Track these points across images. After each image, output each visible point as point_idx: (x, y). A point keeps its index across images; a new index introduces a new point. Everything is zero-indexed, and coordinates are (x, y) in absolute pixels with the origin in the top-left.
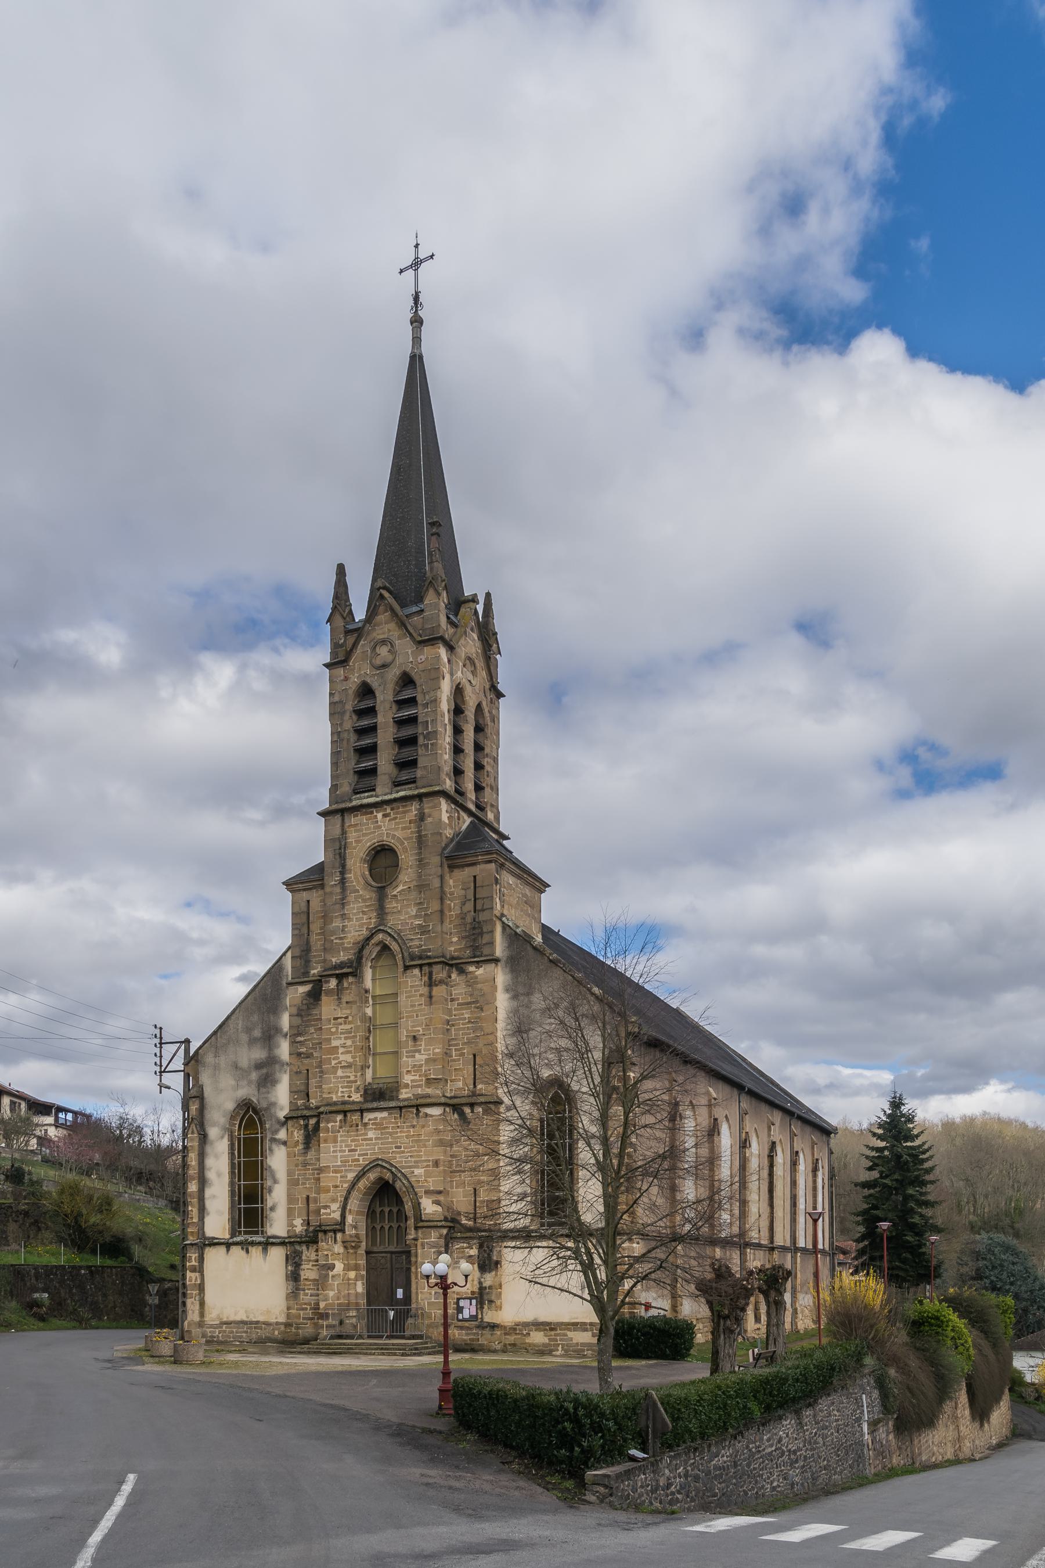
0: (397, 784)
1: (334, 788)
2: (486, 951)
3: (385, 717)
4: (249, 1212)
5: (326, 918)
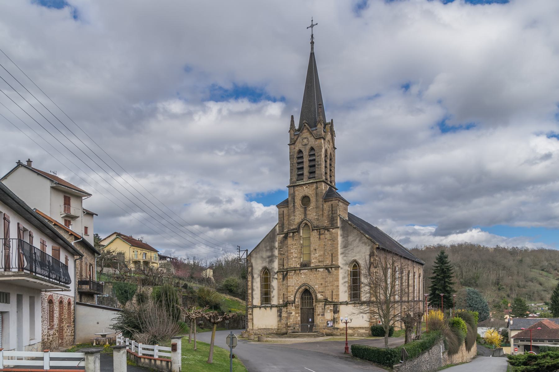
0: (309, 178)
1: (291, 179)
2: (335, 225)
3: (306, 159)
4: (266, 298)
5: (289, 216)
